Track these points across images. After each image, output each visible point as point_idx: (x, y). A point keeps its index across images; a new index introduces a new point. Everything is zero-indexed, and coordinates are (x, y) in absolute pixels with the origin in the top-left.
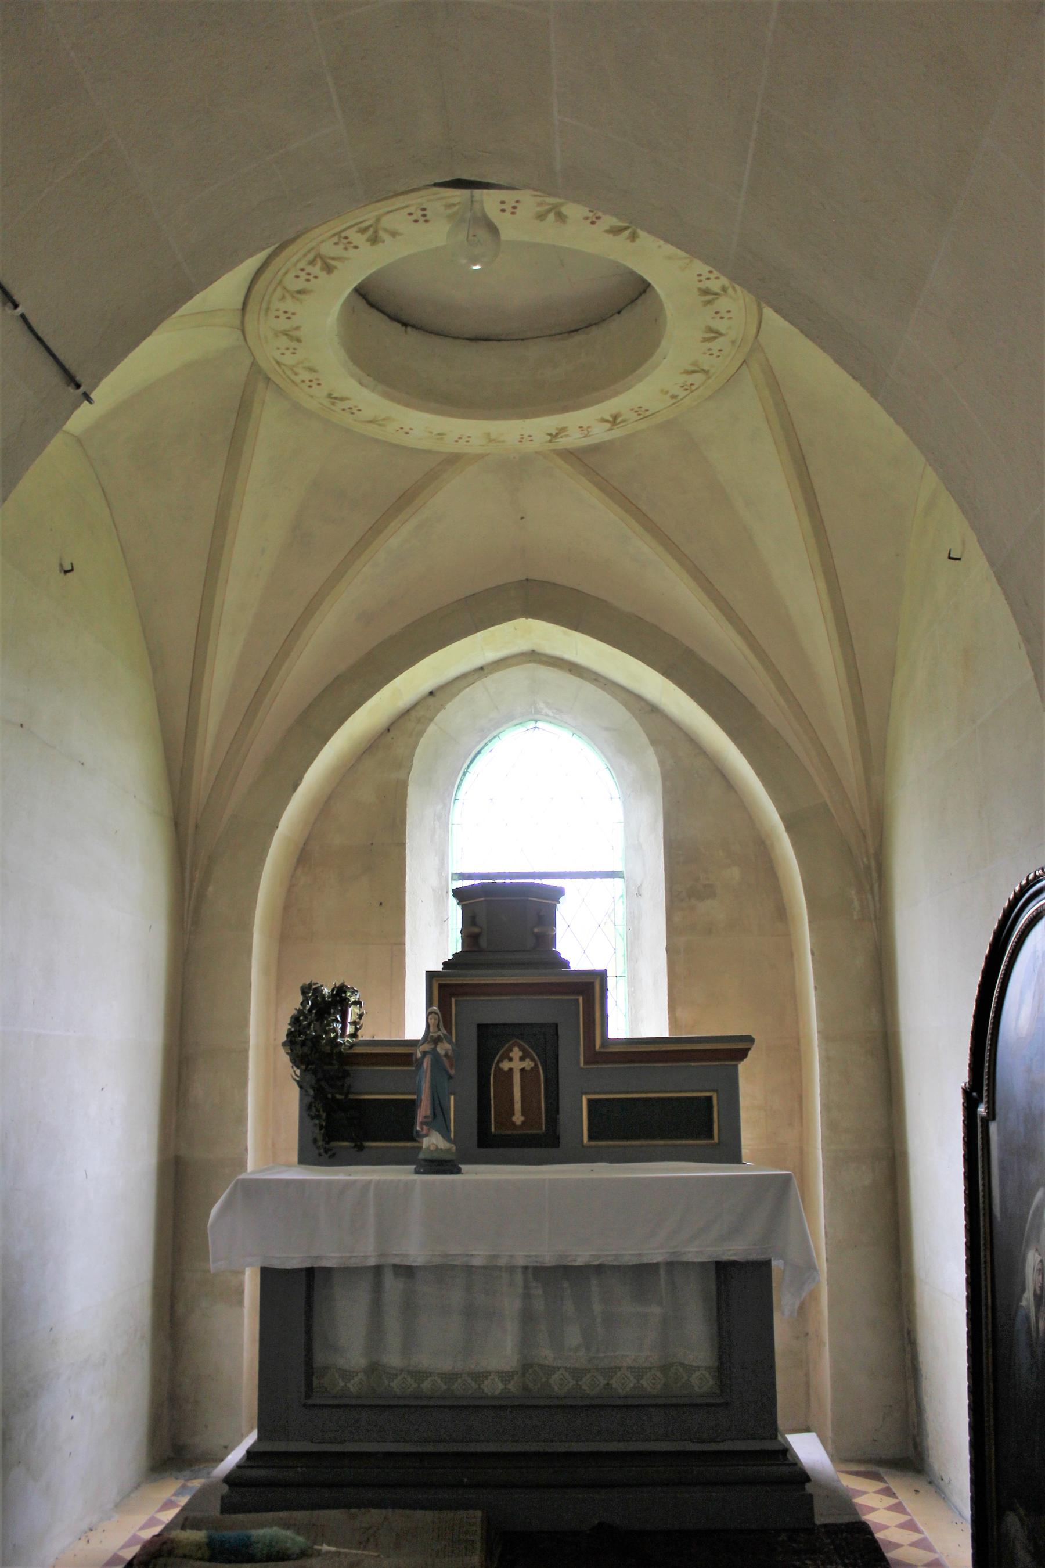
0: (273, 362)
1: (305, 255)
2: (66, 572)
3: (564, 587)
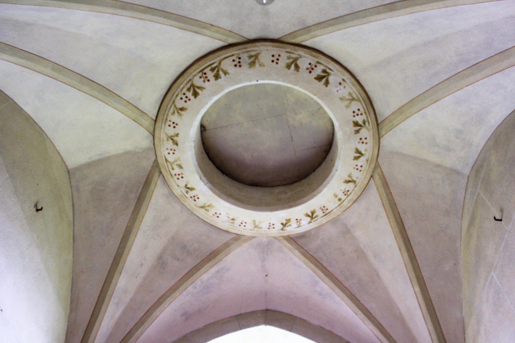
0: (164, 159)
1: (186, 84)
2: (38, 210)
3: (286, 313)
